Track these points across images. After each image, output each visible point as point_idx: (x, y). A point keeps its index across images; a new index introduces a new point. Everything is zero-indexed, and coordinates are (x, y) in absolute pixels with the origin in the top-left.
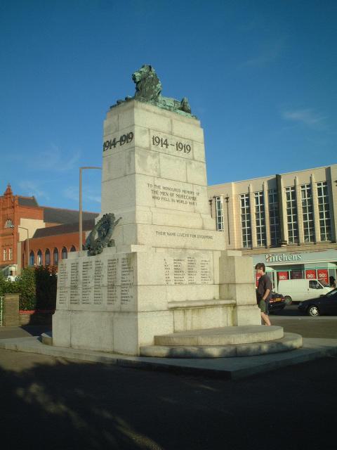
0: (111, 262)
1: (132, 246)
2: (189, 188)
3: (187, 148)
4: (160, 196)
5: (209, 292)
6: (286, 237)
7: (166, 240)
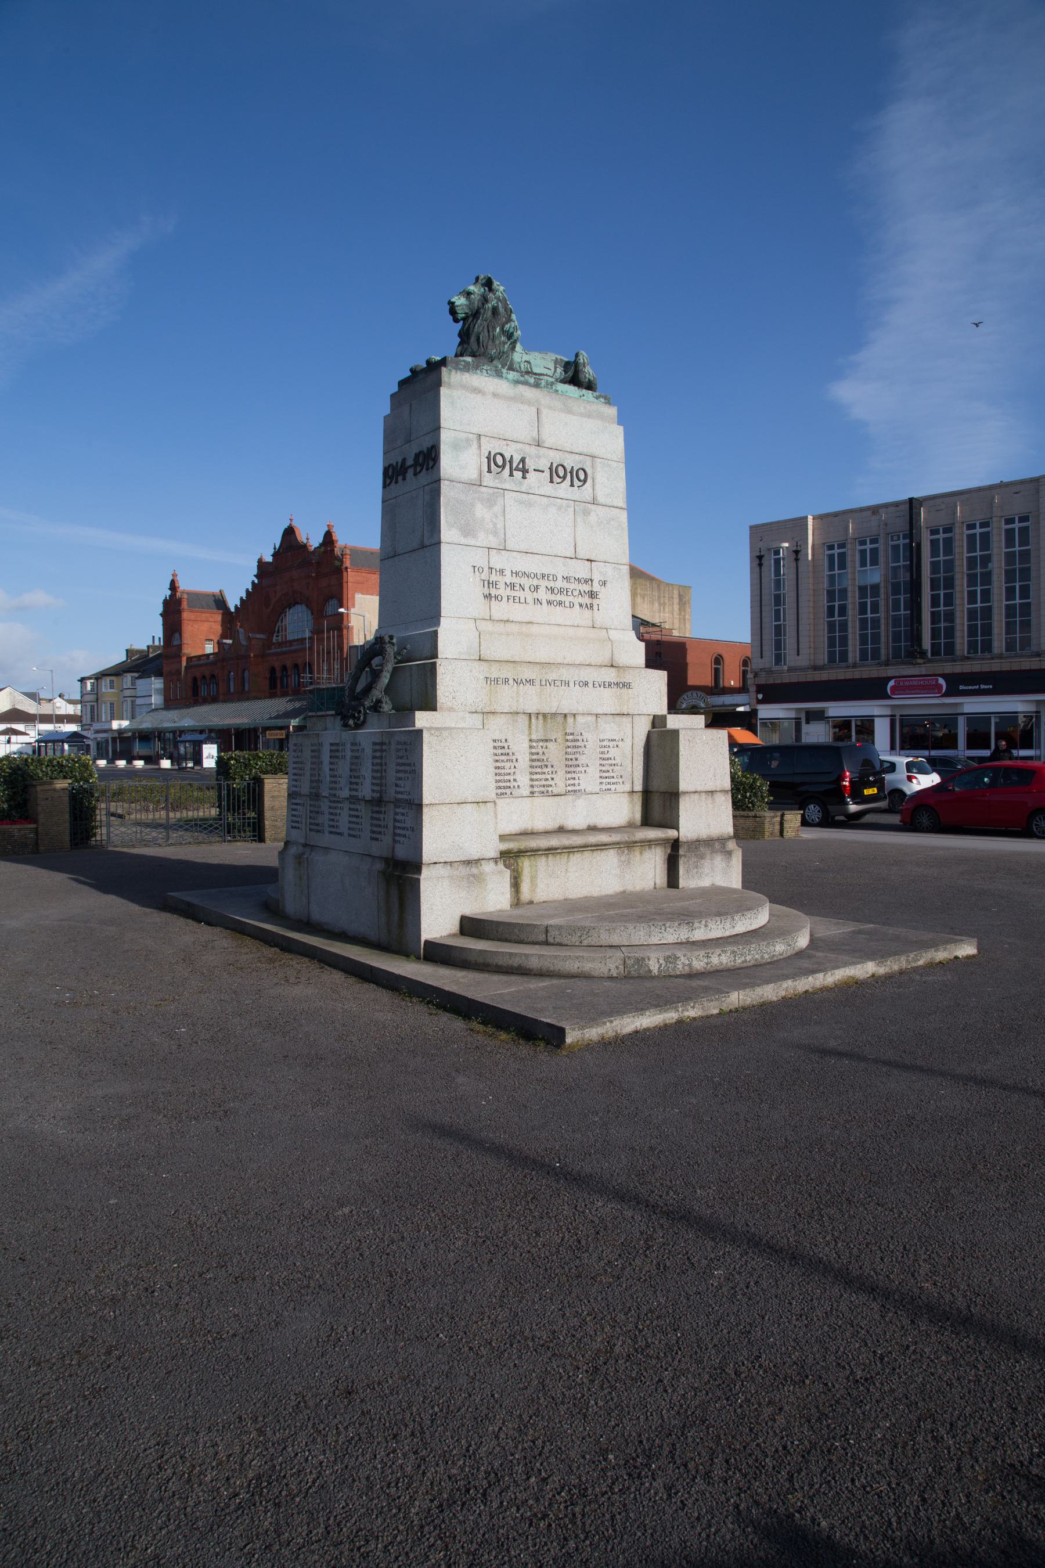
0: (378, 747)
1: (419, 715)
2: (581, 570)
3: (578, 476)
4: (504, 592)
5: (619, 808)
6: (927, 643)
7: (507, 698)
